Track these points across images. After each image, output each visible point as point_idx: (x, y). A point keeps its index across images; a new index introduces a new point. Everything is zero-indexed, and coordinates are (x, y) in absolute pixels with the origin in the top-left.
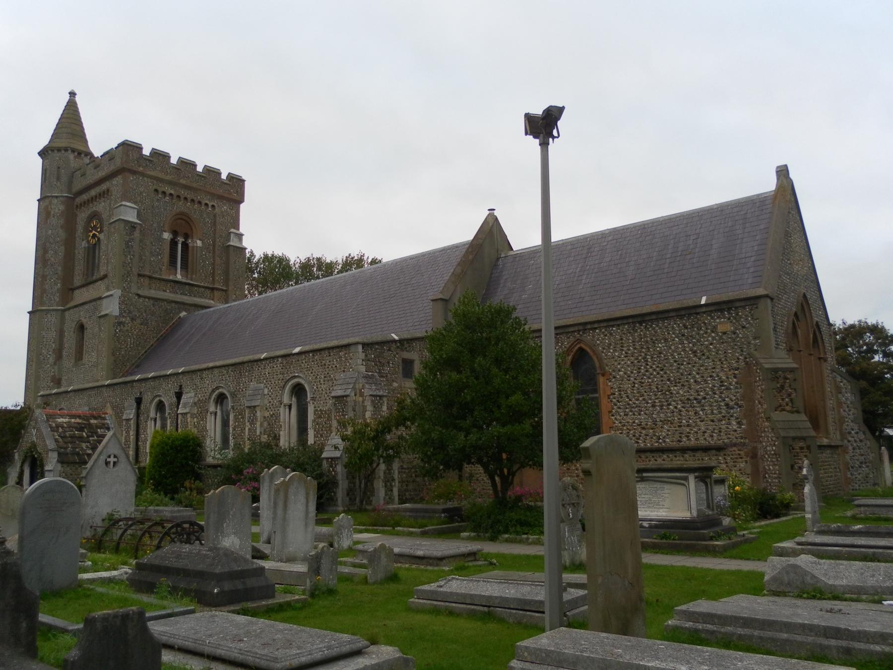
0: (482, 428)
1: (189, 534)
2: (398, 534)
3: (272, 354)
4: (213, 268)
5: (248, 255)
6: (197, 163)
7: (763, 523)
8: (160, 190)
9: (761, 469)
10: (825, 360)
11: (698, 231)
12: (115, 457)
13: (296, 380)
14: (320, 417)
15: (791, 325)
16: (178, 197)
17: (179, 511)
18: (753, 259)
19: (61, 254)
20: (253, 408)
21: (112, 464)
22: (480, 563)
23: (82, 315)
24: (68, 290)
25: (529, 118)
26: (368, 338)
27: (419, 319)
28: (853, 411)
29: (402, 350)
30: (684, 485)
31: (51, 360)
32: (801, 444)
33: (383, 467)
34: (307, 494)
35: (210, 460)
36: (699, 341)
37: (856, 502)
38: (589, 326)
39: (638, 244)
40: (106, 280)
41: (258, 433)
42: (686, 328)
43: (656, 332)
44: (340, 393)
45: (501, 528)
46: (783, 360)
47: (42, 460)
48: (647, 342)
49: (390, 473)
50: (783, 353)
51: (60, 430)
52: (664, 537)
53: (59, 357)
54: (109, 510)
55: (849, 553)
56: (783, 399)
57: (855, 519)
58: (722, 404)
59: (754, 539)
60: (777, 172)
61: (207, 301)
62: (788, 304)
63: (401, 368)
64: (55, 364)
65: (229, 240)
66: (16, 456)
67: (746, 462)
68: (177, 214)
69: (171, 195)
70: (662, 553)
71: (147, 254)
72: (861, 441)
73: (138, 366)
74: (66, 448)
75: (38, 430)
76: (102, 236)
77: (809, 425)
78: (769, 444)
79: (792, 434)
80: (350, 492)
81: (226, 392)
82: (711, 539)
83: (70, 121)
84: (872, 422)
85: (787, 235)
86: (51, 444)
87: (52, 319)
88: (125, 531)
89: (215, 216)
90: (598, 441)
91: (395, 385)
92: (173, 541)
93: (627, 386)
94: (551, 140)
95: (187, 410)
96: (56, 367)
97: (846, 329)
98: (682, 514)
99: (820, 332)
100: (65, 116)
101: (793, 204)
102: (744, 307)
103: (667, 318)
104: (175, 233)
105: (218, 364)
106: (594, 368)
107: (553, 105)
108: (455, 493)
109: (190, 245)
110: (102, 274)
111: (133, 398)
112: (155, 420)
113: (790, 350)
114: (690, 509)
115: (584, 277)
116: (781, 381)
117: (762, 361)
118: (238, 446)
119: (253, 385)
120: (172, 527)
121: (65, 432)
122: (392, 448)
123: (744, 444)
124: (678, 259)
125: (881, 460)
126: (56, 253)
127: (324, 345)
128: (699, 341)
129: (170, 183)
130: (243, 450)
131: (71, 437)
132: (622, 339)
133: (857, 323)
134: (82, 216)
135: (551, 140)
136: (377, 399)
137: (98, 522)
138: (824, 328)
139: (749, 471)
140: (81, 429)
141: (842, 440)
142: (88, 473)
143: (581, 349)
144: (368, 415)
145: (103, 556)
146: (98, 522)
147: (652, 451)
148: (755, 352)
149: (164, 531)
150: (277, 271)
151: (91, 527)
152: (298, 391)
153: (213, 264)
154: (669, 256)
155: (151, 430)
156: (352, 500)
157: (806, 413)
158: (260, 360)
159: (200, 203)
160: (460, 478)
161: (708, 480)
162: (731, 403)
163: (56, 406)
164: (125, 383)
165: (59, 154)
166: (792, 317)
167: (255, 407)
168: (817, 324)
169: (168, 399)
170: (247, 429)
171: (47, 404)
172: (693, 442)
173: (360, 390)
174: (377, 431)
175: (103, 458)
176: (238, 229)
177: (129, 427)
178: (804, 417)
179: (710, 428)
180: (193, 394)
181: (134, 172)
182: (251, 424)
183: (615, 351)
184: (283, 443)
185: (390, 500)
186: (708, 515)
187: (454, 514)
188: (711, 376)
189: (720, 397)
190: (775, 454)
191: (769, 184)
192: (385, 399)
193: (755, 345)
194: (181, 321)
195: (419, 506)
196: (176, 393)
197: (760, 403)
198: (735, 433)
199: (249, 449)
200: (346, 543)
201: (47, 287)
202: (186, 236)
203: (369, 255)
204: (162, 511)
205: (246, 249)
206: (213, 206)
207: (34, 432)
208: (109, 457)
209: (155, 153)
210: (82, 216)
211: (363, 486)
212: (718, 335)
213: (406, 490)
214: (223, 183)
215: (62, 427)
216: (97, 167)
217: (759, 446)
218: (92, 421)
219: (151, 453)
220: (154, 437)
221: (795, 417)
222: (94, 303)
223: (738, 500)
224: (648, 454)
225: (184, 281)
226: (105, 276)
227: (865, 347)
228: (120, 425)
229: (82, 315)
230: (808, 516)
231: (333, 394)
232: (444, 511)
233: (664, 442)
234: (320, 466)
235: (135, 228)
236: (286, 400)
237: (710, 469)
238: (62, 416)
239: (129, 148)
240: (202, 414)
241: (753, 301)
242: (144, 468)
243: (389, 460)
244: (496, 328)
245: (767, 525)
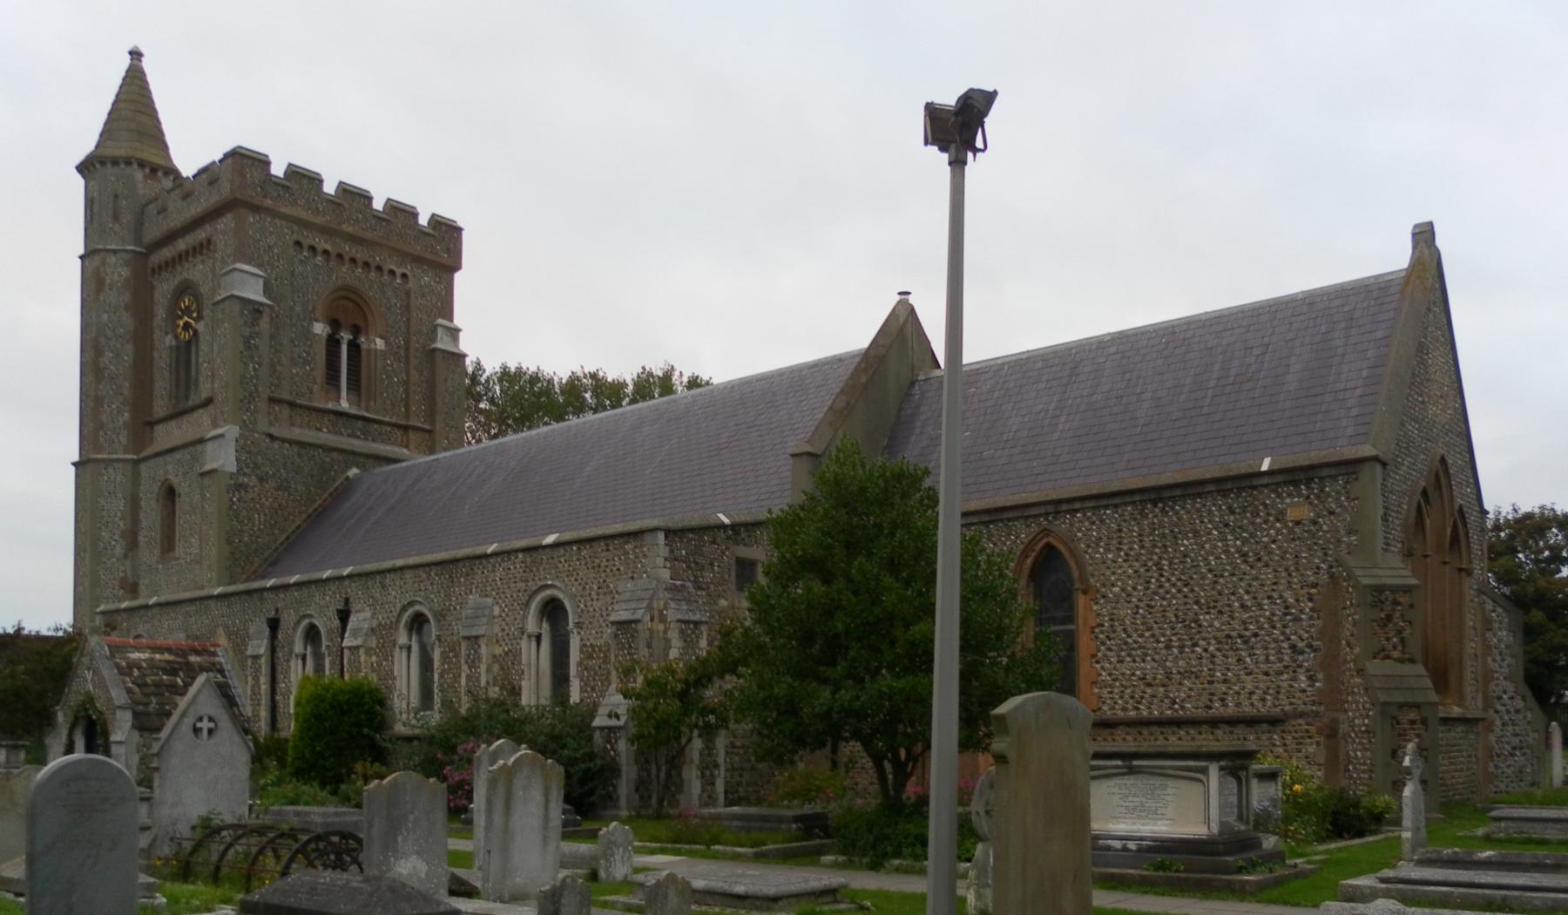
0: (863, 680)
1: (339, 854)
2: (715, 857)
3: (507, 546)
4: (407, 391)
5: (470, 370)
6: (373, 194)
7: (1333, 846)
8: (306, 243)
9: (1342, 756)
10: (1469, 573)
11: (1266, 340)
12: (211, 719)
13: (548, 592)
14: (590, 657)
15: (1413, 513)
16: (340, 256)
17: (337, 814)
18: (1358, 392)
20: (474, 640)
21: (205, 732)
22: (842, 906)
23: (170, 469)
24: (144, 426)
25: (933, 113)
26: (677, 521)
27: (767, 487)
28: (1509, 660)
30: (1200, 781)
31: (119, 550)
32: (1413, 715)
33: (698, 744)
34: (547, 790)
35: (399, 729)
36: (1252, 535)
37: (1494, 814)
38: (1064, 507)
39: (1159, 362)
40: (211, 408)
41: (483, 683)
42: (1233, 512)
43: (1180, 519)
44: (624, 615)
45: (889, 849)
46: (1393, 571)
47: (105, 724)
48: (1164, 536)
49: (710, 755)
50: (1397, 561)
51: (136, 672)
52: (1161, 867)
53: (132, 544)
54: (202, 811)
55: (1463, 897)
56: (1388, 639)
57: (1488, 840)
58: (1285, 645)
59: (1312, 871)
60: (1414, 235)
61: (396, 449)
62: (1413, 473)
63: (733, 573)
64: (126, 556)
65: (434, 340)
66: (60, 717)
67: (1318, 744)
68: (337, 290)
69: (326, 252)
70: (1156, 893)
71: (285, 361)
72: (1517, 711)
73: (274, 564)
74: (146, 705)
75: (96, 672)
76: (200, 327)
77: (1429, 683)
78: (1358, 715)
79: (1399, 698)
80: (641, 786)
81: (426, 611)
82: (1240, 870)
83: (134, 108)
84: (1541, 683)
85: (1422, 349)
86: (119, 696)
87: (117, 478)
88: (230, 845)
89: (408, 294)
90: (1023, 704)
91: (723, 603)
92: (311, 865)
93: (1125, 611)
94: (970, 155)
95: (359, 642)
96: (128, 563)
97: (1517, 521)
98: (1194, 829)
99: (1465, 524)
100: (123, 97)
101: (1438, 294)
102: (1334, 478)
103: (1199, 495)
104: (335, 324)
105: (411, 561)
106: (1071, 581)
107: (976, 87)
108: (819, 789)
109: (364, 347)
110: (204, 395)
111: (264, 619)
112: (304, 658)
113: (1408, 554)
114: (1207, 821)
115: (1063, 419)
116: (1388, 607)
117: (1358, 572)
118: (448, 705)
119: (473, 599)
120: (309, 841)
121: (144, 676)
122: (712, 712)
123: (1317, 714)
124: (1228, 389)
125: (1548, 745)
126: (117, 355)
127: (598, 532)
128: (1252, 535)
129: (324, 231)
130: (457, 711)
131: (157, 685)
132: (1120, 531)
133: (1537, 510)
134: (164, 288)
135: (970, 155)
136: (690, 628)
137: (184, 830)
138: (1472, 518)
139: (1322, 760)
140: (173, 672)
141: (1485, 710)
142: (162, 748)
143: (1049, 546)
144: (674, 653)
145: (191, 887)
146: (184, 830)
147: (1161, 723)
148: (1348, 557)
149: (296, 846)
150: (529, 399)
151: (172, 839)
152: (553, 611)
153: (406, 383)
154: (1212, 383)
155: (296, 674)
156: (645, 799)
157: (1426, 666)
158: (486, 556)
159: (379, 268)
160: (834, 764)
161: (1243, 774)
162: (1300, 645)
163: (129, 631)
164: (249, 592)
165: (116, 170)
166: (1418, 497)
167: (477, 638)
168: (1461, 510)
169: (326, 623)
170: (463, 676)
171: (111, 627)
172: (1231, 710)
173: (661, 612)
174: (686, 682)
175: (188, 722)
176: (451, 319)
177: (257, 670)
178: (1420, 669)
179: (1262, 685)
180: (368, 614)
181: (256, 209)
183: (1108, 550)
184: (527, 699)
185: (710, 800)
186: (1239, 832)
187: (813, 826)
188: (1269, 597)
189: (1283, 633)
190: (1367, 732)
191: (1396, 257)
192: (704, 628)
193: (1349, 545)
194: (349, 486)
195: (753, 810)
196: (339, 611)
197: (1348, 644)
198: (1303, 696)
199: (469, 710)
200: (620, 871)
201: (104, 418)
202: (356, 330)
203: (685, 370)
204: (307, 814)
205: (465, 356)
206: (404, 276)
207: (89, 675)
208: (201, 719)
209: (294, 172)
210: (164, 288)
211: (663, 775)
212: (1286, 526)
213: (739, 784)
214: (422, 232)
215: (139, 668)
216: (186, 196)
217: (1342, 717)
218: (193, 659)
219: (297, 714)
220: (301, 687)
221: (1408, 669)
222: (191, 449)
223: (1298, 806)
224: (1154, 729)
225: (354, 411)
226: (209, 401)
227: (1547, 553)
228: (243, 667)
229: (170, 469)
230: (1407, 835)
231: (613, 617)
232: (797, 819)
233: (1183, 708)
234: (590, 739)
235: (253, 307)
236: (531, 626)
237: (1250, 755)
238: (138, 649)
239: (244, 162)
240: (386, 649)
241: (1351, 467)
242: (286, 740)
243: (708, 732)
244: (892, 505)
245: (1339, 849)
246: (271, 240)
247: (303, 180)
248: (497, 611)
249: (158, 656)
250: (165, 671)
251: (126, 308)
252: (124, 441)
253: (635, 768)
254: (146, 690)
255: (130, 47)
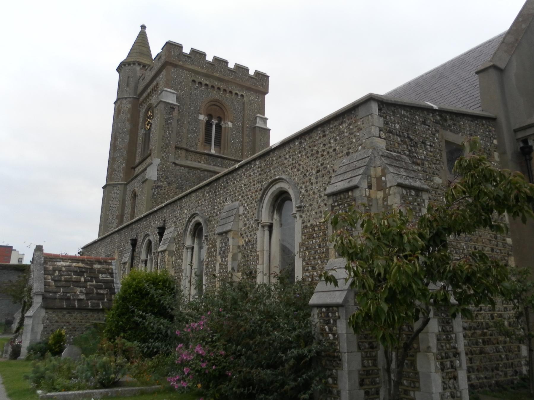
4: (242, 145)
8: (198, 81)
14: (311, 237)
16: (213, 87)
19: (127, 141)
29: (445, 129)
33: (434, 326)
49: (448, 340)
65: (256, 123)
69: (206, 85)
74: (55, 293)
87: (117, 191)
89: (244, 103)
104: (210, 116)
109: (223, 126)
119: (228, 205)
121: (61, 275)
129: (206, 76)
131: (66, 281)
159: (231, 92)
165: (129, 67)
167: (226, 232)
173: (379, 179)
176: (264, 115)
181: (175, 66)
182: (222, 257)
201: (115, 167)
202: (220, 119)
206: (242, 96)
214: (251, 77)
218: (97, 266)
225: (217, 154)
236: (265, 218)
246: (181, 79)
247: (197, 55)
248: (241, 209)
249: (74, 264)
250: (76, 273)
251: (128, 120)
252: (122, 175)
253: (358, 357)
254: (59, 284)
255: (141, 24)
